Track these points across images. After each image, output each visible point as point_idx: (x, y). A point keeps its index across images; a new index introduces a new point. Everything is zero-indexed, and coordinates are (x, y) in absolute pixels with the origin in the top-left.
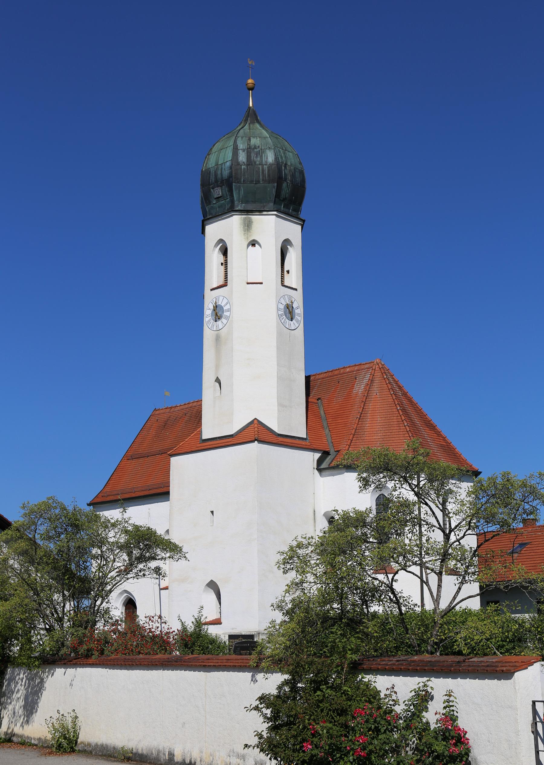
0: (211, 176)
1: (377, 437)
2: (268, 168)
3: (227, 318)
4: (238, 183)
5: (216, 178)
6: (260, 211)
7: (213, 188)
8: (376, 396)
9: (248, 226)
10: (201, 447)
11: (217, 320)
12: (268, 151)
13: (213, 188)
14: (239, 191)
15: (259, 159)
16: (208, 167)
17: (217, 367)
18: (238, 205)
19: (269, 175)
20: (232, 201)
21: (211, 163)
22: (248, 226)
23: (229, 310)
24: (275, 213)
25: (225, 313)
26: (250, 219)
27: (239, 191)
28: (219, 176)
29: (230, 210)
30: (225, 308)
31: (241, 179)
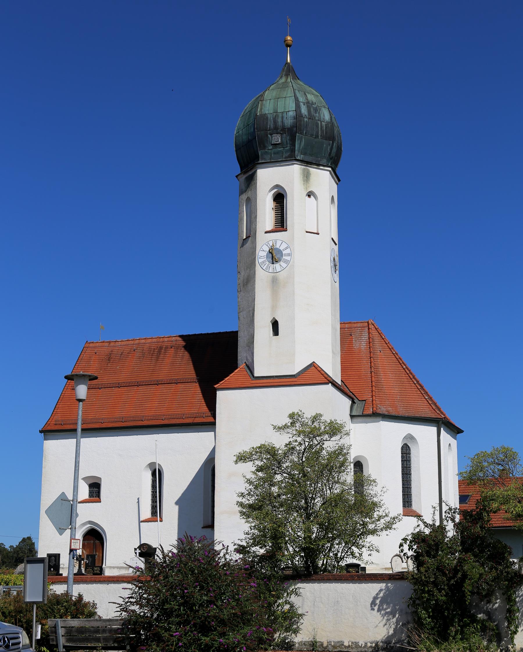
0: (269, 122)
1: (395, 391)
2: (326, 125)
3: (287, 262)
4: (301, 134)
5: (276, 125)
6: (318, 165)
7: (271, 134)
8: (381, 354)
9: (306, 177)
10: (274, 383)
11: (274, 262)
12: (323, 109)
13: (271, 134)
14: (301, 142)
15: (317, 115)
16: (263, 113)
17: (274, 308)
18: (298, 155)
19: (326, 133)
20: (293, 150)
21: (267, 108)
22: (306, 177)
23: (289, 255)
24: (330, 169)
25: (284, 257)
26: (308, 170)
27: (301, 142)
28: (280, 123)
29: (290, 158)
30: (284, 252)
31: (304, 131)
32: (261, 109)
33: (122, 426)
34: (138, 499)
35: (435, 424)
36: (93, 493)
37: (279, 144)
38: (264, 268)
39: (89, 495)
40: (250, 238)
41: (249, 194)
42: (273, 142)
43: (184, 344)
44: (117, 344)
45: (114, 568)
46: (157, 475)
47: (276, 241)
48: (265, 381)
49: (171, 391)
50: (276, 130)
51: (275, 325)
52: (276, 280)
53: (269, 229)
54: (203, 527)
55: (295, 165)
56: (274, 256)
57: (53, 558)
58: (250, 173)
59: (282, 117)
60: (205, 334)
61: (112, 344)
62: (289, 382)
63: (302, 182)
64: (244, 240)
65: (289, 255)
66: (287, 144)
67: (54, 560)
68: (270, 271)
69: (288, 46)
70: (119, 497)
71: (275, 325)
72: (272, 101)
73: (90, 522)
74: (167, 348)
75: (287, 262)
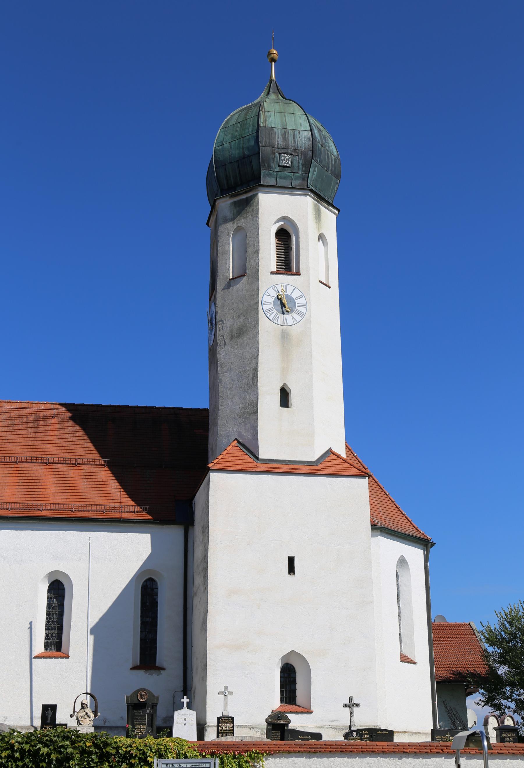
3: (300, 314)
17: (285, 371)
23: (304, 306)
25: (297, 308)
29: (302, 187)
30: (297, 302)
32: (265, 121)
34: (31, 623)
35: (422, 547)
38: (271, 318)
40: (245, 278)
41: (242, 222)
42: (282, 163)
43: (68, 414)
46: (58, 590)
47: (286, 286)
49: (70, 473)
50: (286, 150)
52: (288, 335)
53: (274, 269)
54: (131, 669)
55: (308, 197)
56: (283, 305)
58: (244, 197)
59: (294, 136)
60: (98, 406)
62: (314, 470)
63: (315, 221)
64: (230, 279)
65: (304, 306)
66: (298, 169)
68: (279, 323)
69: (273, 60)
72: (277, 114)
74: (45, 417)
75: (300, 314)
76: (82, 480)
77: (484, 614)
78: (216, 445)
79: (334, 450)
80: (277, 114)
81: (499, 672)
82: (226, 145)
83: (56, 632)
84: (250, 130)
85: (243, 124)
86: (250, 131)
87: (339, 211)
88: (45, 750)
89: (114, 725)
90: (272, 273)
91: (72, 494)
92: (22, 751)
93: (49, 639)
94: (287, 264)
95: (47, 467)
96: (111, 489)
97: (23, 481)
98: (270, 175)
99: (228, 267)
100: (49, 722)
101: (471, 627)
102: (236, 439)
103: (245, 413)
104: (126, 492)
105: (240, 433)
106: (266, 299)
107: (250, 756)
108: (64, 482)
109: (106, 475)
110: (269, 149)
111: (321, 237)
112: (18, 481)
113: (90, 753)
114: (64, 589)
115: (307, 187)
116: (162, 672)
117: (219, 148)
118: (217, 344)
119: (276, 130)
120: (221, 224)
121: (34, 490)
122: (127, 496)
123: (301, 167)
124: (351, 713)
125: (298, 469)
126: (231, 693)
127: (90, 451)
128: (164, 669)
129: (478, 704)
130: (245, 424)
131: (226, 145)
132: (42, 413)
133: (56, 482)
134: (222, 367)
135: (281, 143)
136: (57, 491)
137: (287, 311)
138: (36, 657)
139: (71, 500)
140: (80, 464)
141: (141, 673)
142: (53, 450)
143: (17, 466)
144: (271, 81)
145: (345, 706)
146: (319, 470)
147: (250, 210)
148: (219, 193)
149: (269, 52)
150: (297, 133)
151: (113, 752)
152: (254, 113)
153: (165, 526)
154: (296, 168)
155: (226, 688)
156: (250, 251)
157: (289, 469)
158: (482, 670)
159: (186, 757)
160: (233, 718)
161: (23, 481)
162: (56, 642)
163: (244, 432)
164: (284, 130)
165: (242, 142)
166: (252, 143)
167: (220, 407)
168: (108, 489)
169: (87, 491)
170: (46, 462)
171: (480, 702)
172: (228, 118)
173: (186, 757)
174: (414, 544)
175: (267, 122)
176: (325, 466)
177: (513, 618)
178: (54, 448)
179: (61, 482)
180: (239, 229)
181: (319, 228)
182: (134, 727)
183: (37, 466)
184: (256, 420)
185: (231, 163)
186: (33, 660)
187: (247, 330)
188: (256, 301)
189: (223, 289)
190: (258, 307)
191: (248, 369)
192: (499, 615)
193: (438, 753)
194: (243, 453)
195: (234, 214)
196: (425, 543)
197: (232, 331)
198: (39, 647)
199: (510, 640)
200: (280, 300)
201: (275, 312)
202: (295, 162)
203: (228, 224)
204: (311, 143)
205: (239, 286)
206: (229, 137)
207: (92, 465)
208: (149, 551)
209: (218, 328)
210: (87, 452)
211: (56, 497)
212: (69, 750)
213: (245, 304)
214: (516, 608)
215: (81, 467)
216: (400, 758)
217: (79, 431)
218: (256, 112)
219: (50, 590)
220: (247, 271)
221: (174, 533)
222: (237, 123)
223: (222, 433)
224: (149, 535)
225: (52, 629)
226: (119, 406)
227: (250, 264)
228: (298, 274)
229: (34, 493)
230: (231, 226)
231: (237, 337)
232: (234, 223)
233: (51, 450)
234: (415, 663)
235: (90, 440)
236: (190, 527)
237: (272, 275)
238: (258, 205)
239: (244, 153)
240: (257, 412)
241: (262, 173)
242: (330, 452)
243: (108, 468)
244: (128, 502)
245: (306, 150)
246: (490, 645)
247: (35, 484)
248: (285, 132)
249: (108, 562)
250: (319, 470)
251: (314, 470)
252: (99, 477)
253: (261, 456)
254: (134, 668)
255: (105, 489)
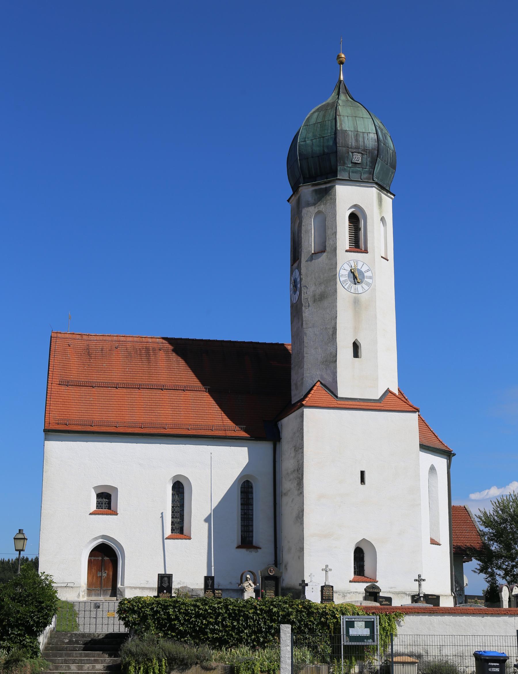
3: (368, 284)
17: (356, 329)
23: (370, 278)
25: (365, 279)
28: (361, 143)
30: (366, 274)
32: (341, 124)
33: (140, 432)
35: (446, 457)
36: (102, 503)
37: (359, 164)
38: (346, 287)
39: (97, 506)
40: (325, 254)
41: (322, 207)
42: (354, 161)
43: (171, 347)
44: (92, 338)
45: (135, 588)
48: (350, 403)
49: (181, 398)
51: (356, 347)
52: (358, 301)
53: (348, 248)
56: (355, 277)
57: (166, 579)
58: (323, 186)
59: (363, 138)
60: (193, 340)
61: (85, 337)
63: (378, 207)
64: (312, 254)
65: (370, 278)
66: (367, 165)
67: (167, 581)
69: (341, 63)
70: (125, 510)
71: (356, 347)
72: (350, 118)
73: (103, 537)
74: (154, 349)
75: (368, 284)
76: (190, 403)
77: (482, 502)
78: (302, 383)
79: (391, 389)
80: (350, 118)
81: (493, 548)
82: (308, 142)
83: (178, 520)
84: (329, 131)
85: (322, 124)
86: (329, 133)
87: (394, 195)
88: (275, 610)
89: (225, 588)
90: (347, 251)
91: (185, 415)
92: (261, 610)
93: (174, 525)
94: (357, 244)
95: (163, 392)
96: (213, 411)
97: (146, 404)
98: (344, 170)
99: (310, 242)
100: (210, 588)
101: (466, 509)
102: (319, 381)
103: (326, 361)
104: (225, 413)
105: (322, 376)
106: (343, 272)
107: (395, 614)
108: (177, 405)
109: (208, 399)
110: (344, 149)
111: (383, 219)
112: (143, 404)
113: (301, 612)
114: (183, 488)
115: (373, 180)
116: (259, 550)
117: (302, 143)
118: (302, 305)
119: (350, 133)
120: (304, 207)
121: (156, 412)
122: (226, 417)
123: (368, 163)
124: (420, 585)
125: (367, 406)
126: (330, 570)
127: (193, 381)
128: (261, 548)
129: (475, 572)
130: (326, 369)
131: (308, 142)
132: (151, 346)
133: (172, 405)
134: (306, 324)
135: (353, 144)
136: (174, 412)
137: (358, 282)
138: (167, 538)
139: (185, 420)
140: (187, 390)
141: (243, 551)
142: (165, 378)
143: (140, 391)
144: (340, 81)
145: (416, 580)
146: (382, 407)
147: (329, 198)
148: (301, 180)
149: (338, 56)
150: (366, 135)
151: (315, 611)
152: (331, 116)
153: (259, 442)
154: (365, 164)
155: (327, 566)
156: (329, 232)
157: (361, 406)
158: (477, 546)
159: (358, 615)
160: (332, 587)
161: (146, 404)
162: (179, 528)
163: (325, 376)
164: (356, 133)
165: (322, 141)
166: (331, 143)
167: (305, 355)
168: (211, 411)
169: (196, 413)
170: (162, 389)
171: (476, 571)
172: (308, 116)
173: (358, 615)
174: (440, 455)
175: (343, 126)
176: (385, 404)
177: (504, 507)
178: (165, 376)
179: (175, 405)
180: (319, 212)
181: (381, 213)
182: (266, 592)
183: (155, 391)
184: (336, 367)
185: (313, 157)
186: (165, 540)
187: (327, 296)
188: (334, 274)
189: (307, 261)
190: (336, 278)
191: (328, 327)
192: (494, 504)
193: (505, 614)
194: (325, 392)
195: (315, 200)
196: (448, 454)
197: (314, 296)
198: (168, 532)
199: (501, 524)
200: (353, 273)
201: (349, 283)
202: (364, 159)
203: (310, 208)
204: (376, 143)
205: (320, 260)
206: (310, 135)
207: (196, 391)
208: (247, 461)
209: (302, 292)
210: (191, 380)
211: (174, 417)
212: (290, 610)
213: (326, 275)
214: (508, 498)
215: (188, 393)
216: (483, 617)
217: (182, 362)
218: (333, 116)
219: (174, 488)
220: (326, 247)
221: (266, 447)
222: (317, 123)
223: (308, 375)
224: (246, 449)
225: (176, 518)
226: (209, 341)
227: (329, 243)
228: (366, 251)
229: (156, 414)
230: (312, 210)
231: (319, 301)
232: (315, 208)
233: (163, 378)
234: (439, 544)
235: (191, 369)
236: (278, 443)
237: (347, 253)
238: (335, 195)
239: (324, 151)
240: (336, 361)
241: (339, 169)
242: (388, 391)
243: (209, 394)
244: (228, 422)
245: (374, 149)
246: (486, 527)
247: (156, 407)
248: (357, 135)
249: (218, 468)
250: (382, 407)
251: (379, 406)
252: (203, 401)
253: (340, 395)
254: (238, 547)
255: (210, 411)
